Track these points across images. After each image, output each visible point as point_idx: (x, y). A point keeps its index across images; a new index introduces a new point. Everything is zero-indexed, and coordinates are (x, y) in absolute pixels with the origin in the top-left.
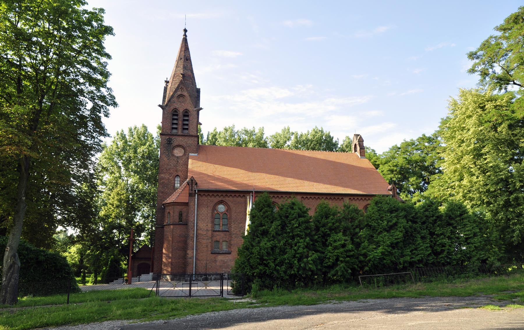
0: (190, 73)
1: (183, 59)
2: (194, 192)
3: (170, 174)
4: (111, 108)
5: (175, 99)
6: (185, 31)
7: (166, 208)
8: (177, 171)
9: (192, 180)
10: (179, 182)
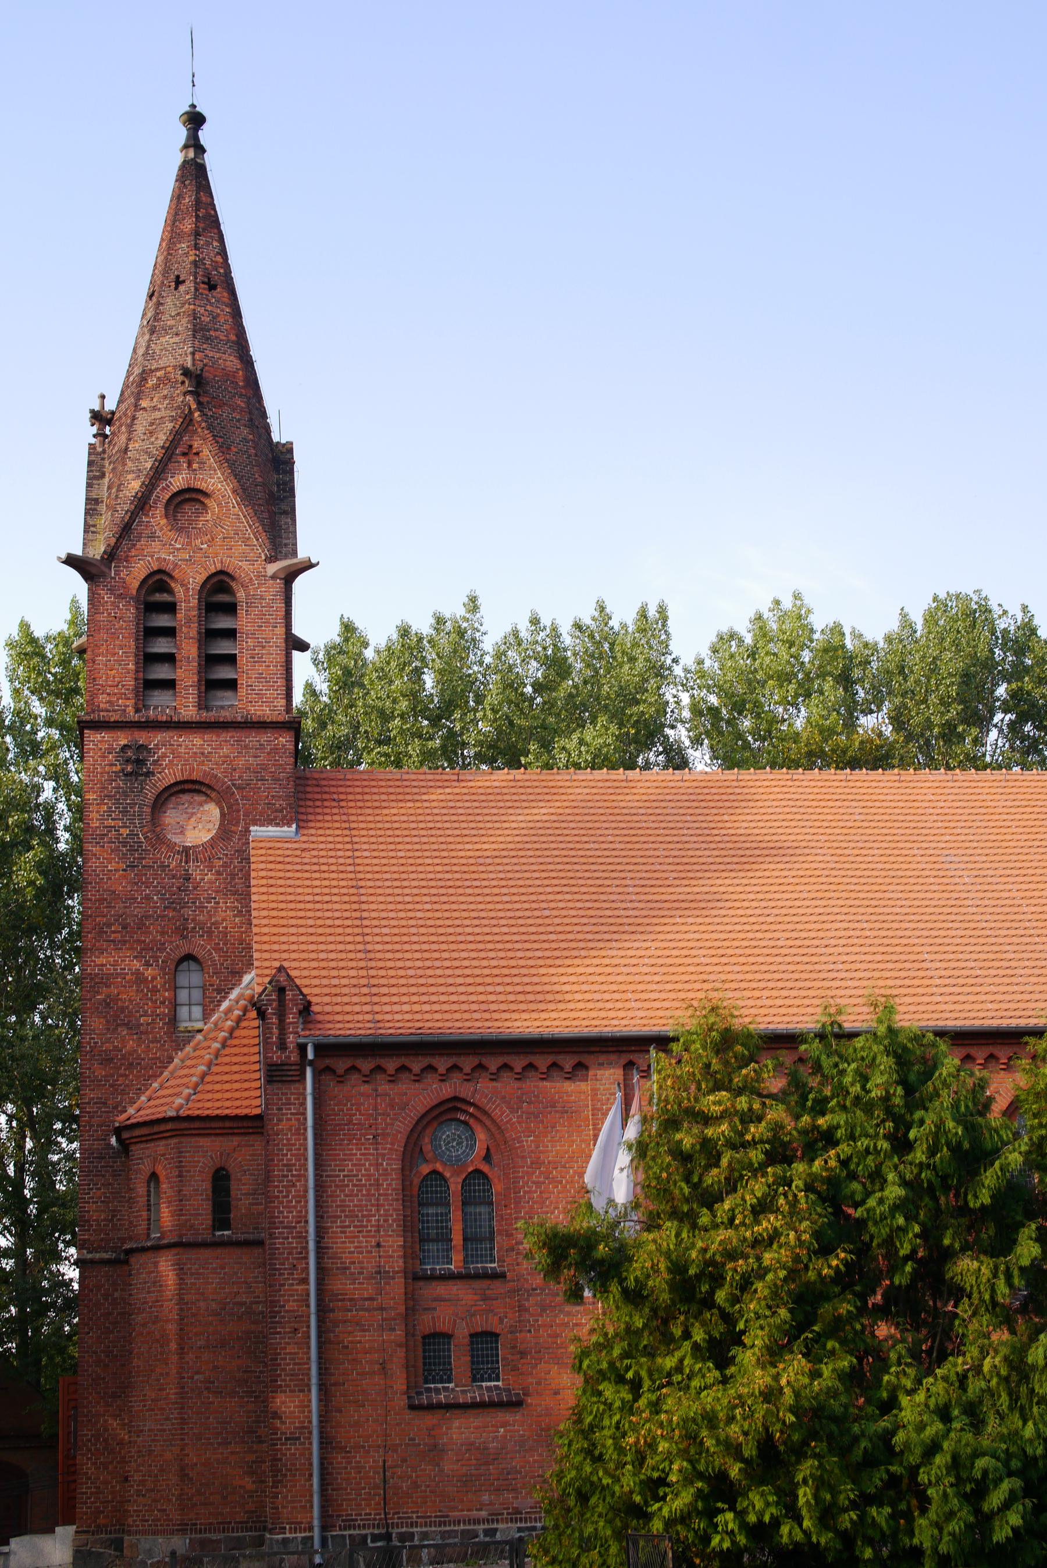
0: (231, 362)
1: (189, 285)
2: (294, 1057)
3: (146, 951)
4: (587, 621)
5: (157, 519)
6: (195, 120)
7: (136, 1150)
8: (182, 932)
9: (282, 991)
10: (197, 995)
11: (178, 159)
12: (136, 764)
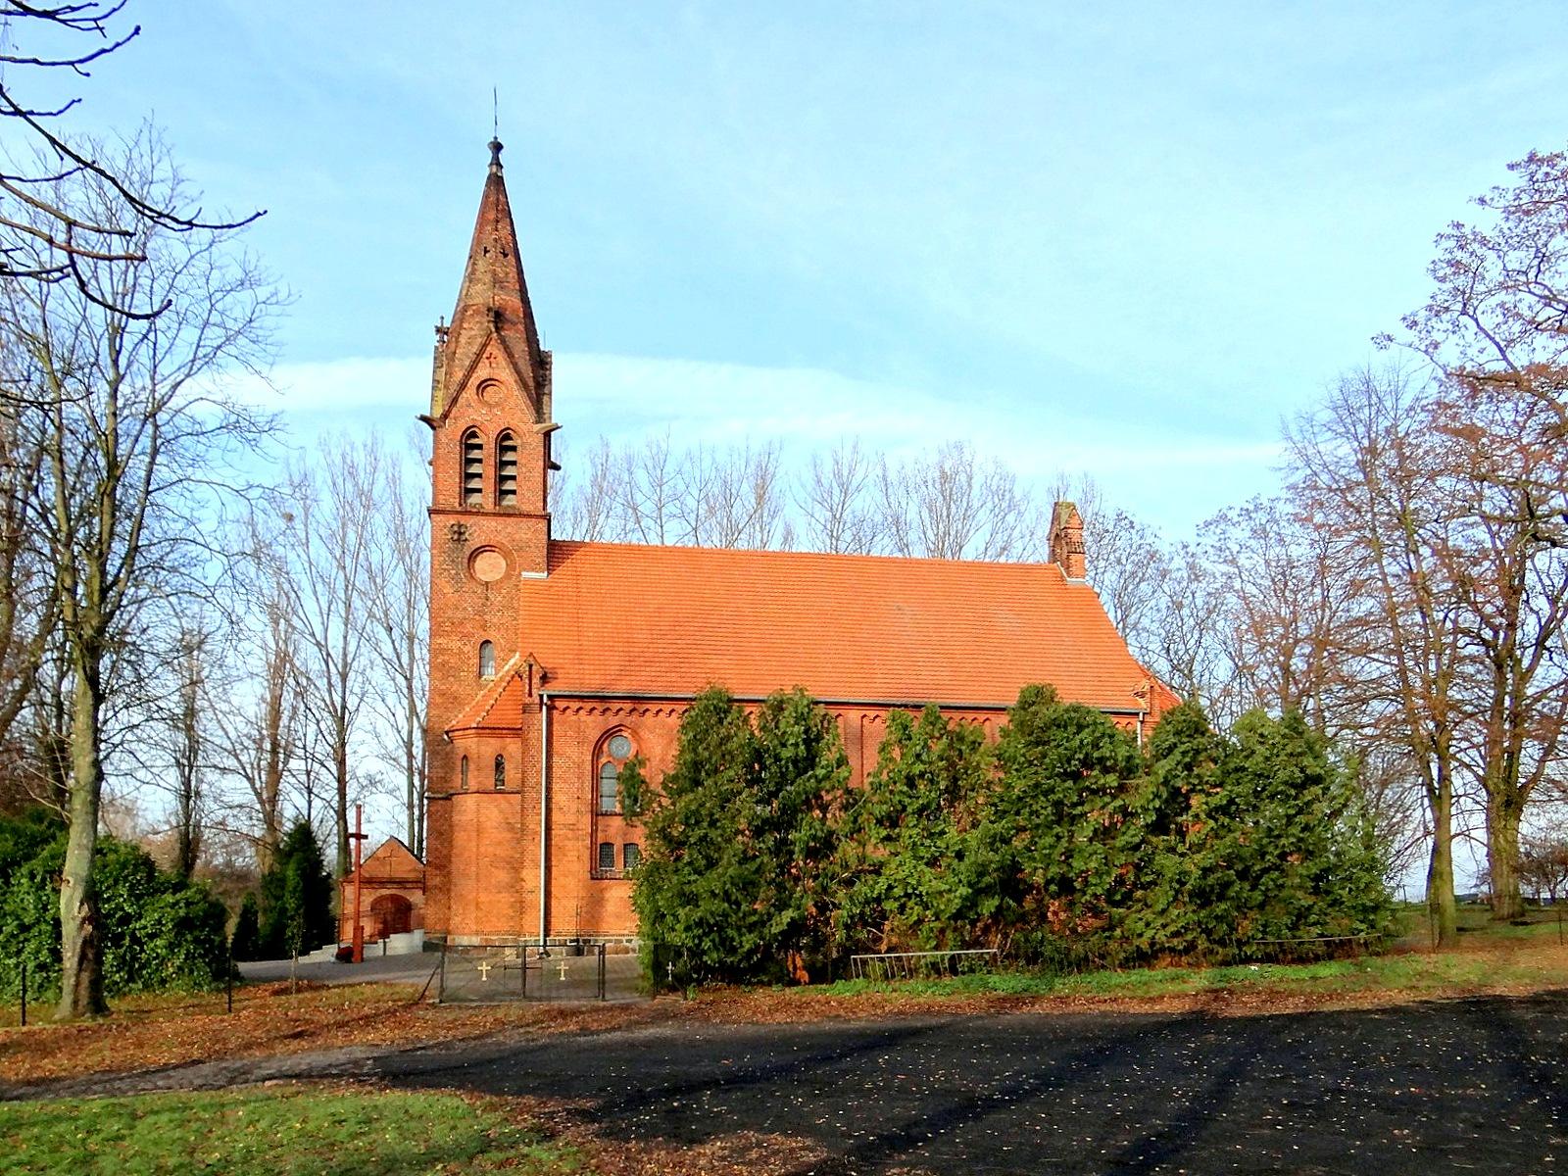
2: (537, 701)
5: (470, 394)
6: (497, 147)
11: (487, 172)
12: (459, 534)
